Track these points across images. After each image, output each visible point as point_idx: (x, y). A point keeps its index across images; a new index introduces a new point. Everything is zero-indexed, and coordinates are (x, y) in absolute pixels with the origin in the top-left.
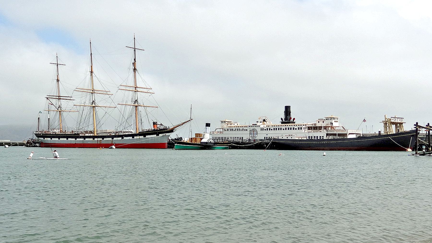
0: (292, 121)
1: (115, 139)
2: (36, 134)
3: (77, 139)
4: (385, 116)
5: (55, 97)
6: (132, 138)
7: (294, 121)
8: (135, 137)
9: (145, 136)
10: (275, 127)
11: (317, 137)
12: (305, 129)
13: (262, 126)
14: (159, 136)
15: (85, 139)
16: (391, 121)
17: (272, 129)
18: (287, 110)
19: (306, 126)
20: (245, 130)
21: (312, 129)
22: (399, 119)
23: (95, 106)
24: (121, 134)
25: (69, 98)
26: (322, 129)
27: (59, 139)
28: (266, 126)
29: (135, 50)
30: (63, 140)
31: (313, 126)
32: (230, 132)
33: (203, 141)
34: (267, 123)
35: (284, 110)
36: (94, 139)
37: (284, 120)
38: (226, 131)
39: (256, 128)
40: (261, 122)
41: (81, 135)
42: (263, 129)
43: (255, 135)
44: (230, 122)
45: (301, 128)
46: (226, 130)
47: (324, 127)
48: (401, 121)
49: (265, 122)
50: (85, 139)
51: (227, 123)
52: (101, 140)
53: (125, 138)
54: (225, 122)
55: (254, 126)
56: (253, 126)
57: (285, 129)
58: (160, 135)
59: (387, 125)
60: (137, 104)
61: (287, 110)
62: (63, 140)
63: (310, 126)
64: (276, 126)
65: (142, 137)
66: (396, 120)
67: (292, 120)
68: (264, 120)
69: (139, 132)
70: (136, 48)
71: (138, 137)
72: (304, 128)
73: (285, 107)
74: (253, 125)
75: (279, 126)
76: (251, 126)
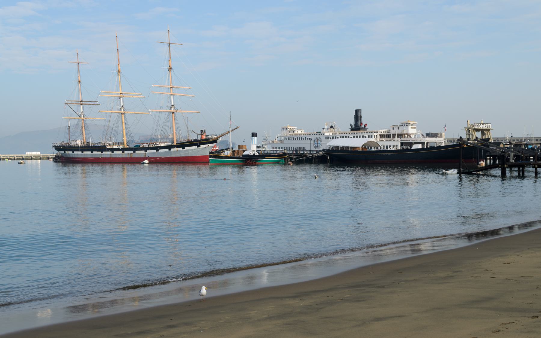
0: (364, 127)
1: (148, 151)
2: (56, 147)
3: (104, 152)
4: (468, 122)
5: (74, 102)
6: (182, 149)
7: (366, 127)
8: (172, 150)
9: (183, 148)
10: (370, 135)
11: (384, 146)
12: (376, 137)
13: (327, 134)
14: (200, 147)
15: (113, 152)
16: (475, 128)
17: (304, 139)
18: (358, 116)
19: (377, 133)
20: (308, 139)
21: (384, 137)
22: (485, 124)
23: (124, 112)
24: (156, 146)
25: (93, 103)
26: (396, 137)
27: (82, 152)
28: (333, 134)
29: (169, 45)
30: (88, 154)
31: (387, 133)
32: (292, 141)
33: (245, 153)
34: (335, 130)
35: (354, 114)
36: (123, 152)
37: (353, 127)
38: (296, 139)
39: (320, 136)
40: (328, 129)
41: (108, 147)
42: (328, 137)
43: (319, 145)
44: (293, 129)
45: (372, 137)
46: (286, 139)
47: (399, 134)
48: (488, 127)
49: (333, 129)
50: (113, 153)
51: (289, 131)
52: (132, 154)
53: (160, 150)
54: (287, 129)
55: (358, 133)
56: (317, 134)
57: (332, 139)
58: (202, 146)
59: (471, 132)
60: (174, 109)
61: (358, 116)
62: (88, 154)
63: (383, 133)
64: (369, 133)
65: (180, 149)
66: (481, 127)
67: (363, 126)
68: (332, 127)
69: (177, 144)
70: (170, 43)
71: (175, 149)
72: (376, 136)
73: (354, 111)
74: (317, 133)
75: (347, 134)
76: (315, 134)
